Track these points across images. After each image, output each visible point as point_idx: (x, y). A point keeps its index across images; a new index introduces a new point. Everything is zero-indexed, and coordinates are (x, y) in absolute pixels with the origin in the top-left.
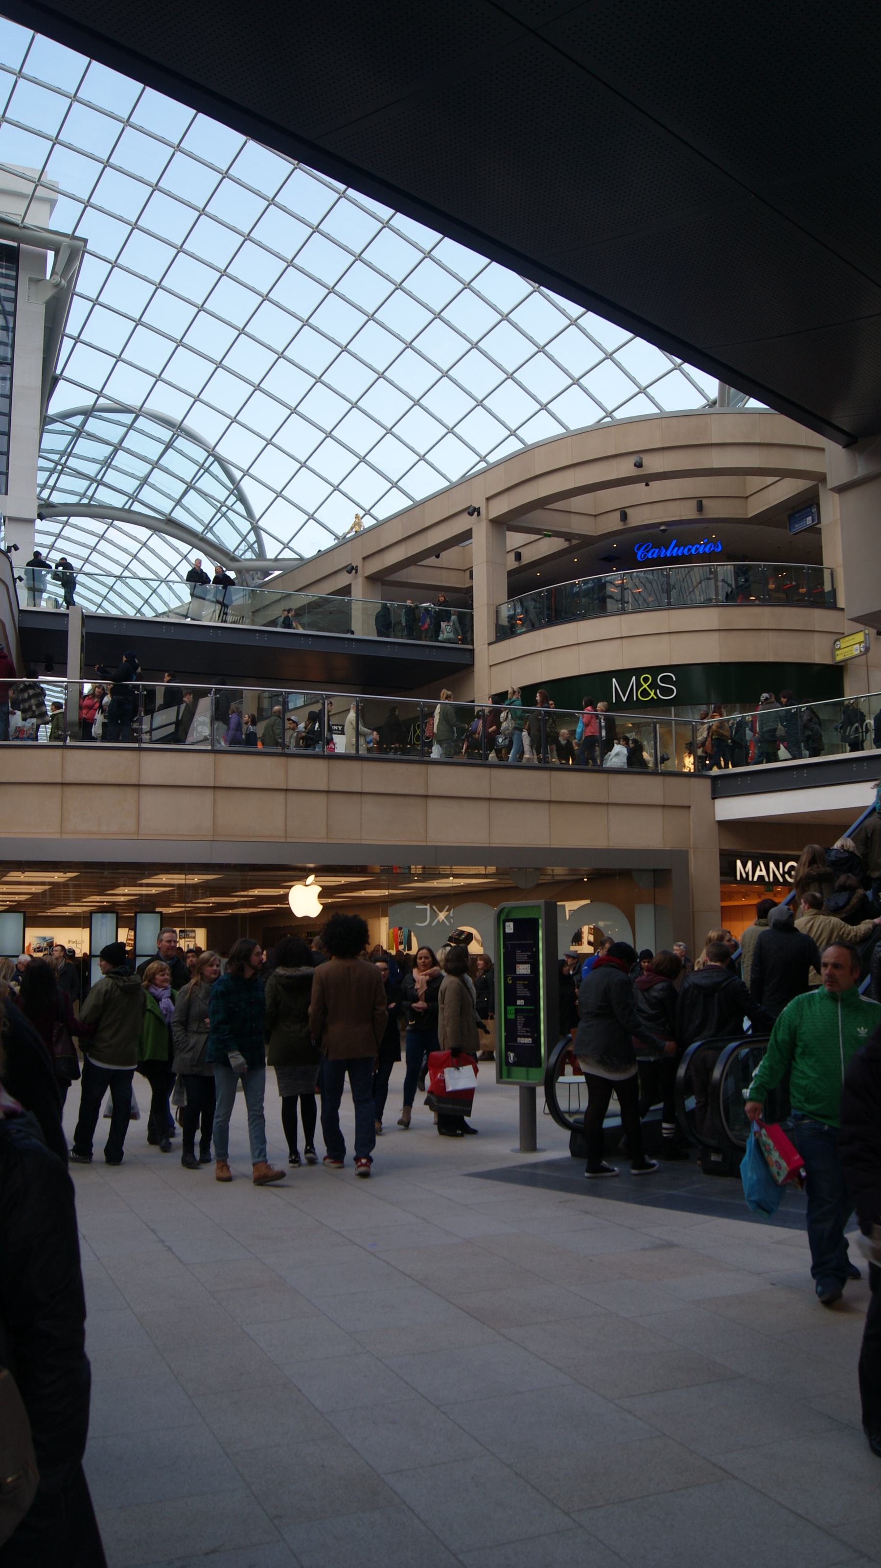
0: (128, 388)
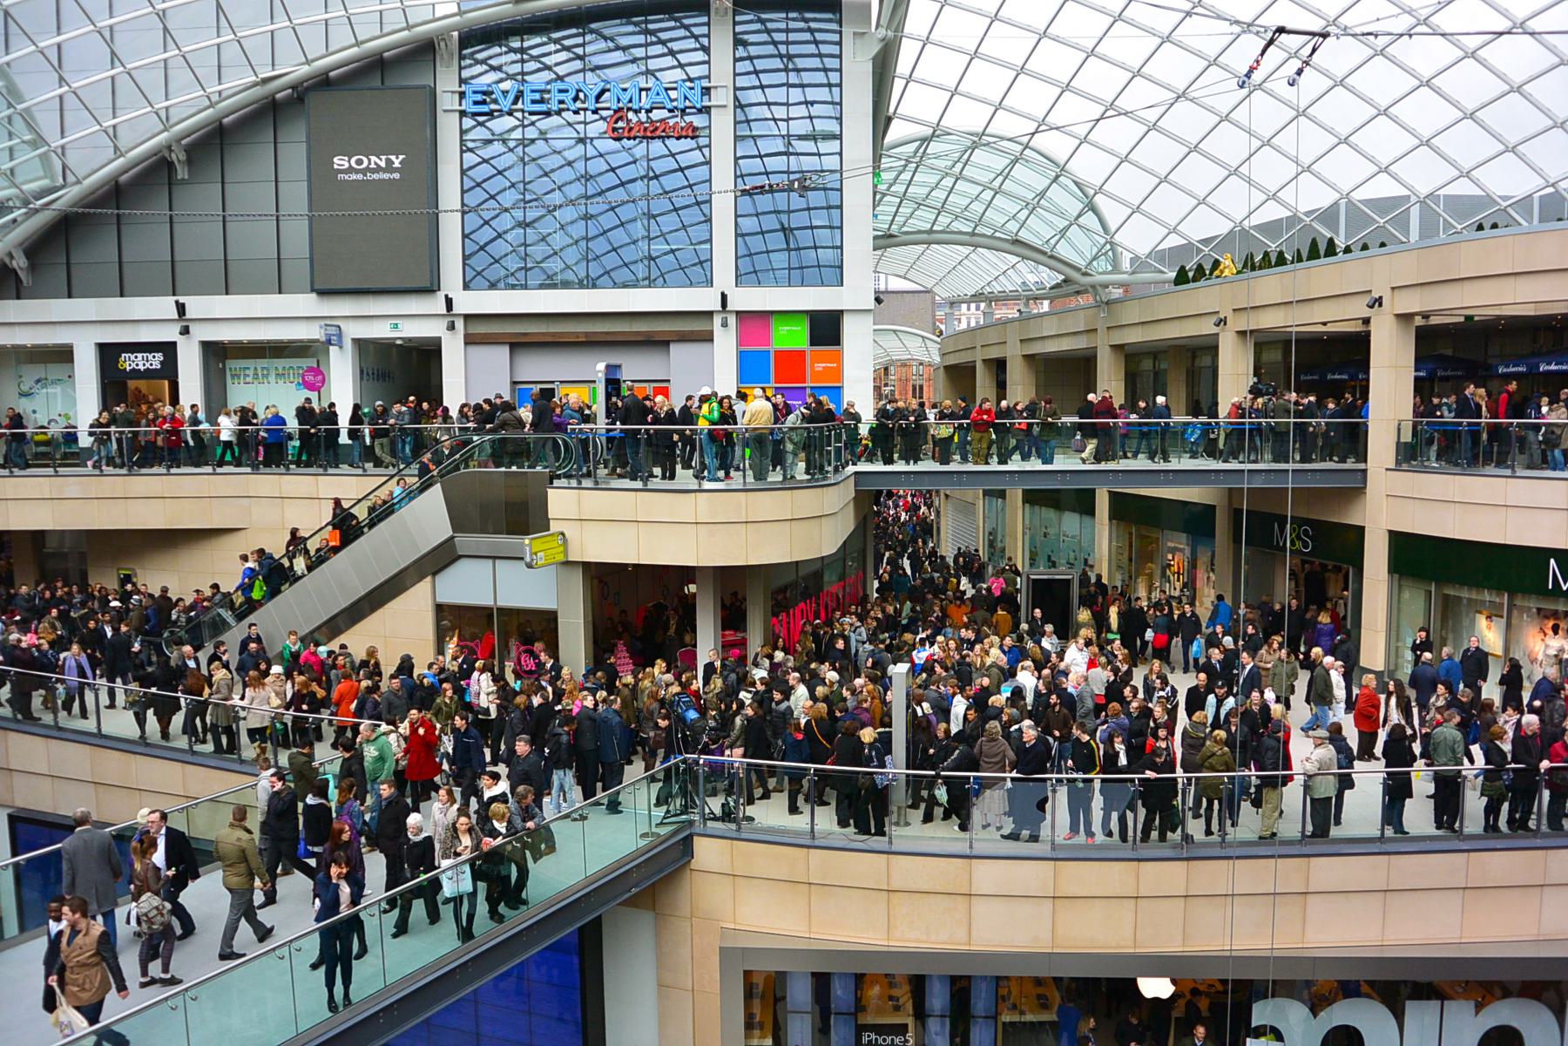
0: (966, 117)
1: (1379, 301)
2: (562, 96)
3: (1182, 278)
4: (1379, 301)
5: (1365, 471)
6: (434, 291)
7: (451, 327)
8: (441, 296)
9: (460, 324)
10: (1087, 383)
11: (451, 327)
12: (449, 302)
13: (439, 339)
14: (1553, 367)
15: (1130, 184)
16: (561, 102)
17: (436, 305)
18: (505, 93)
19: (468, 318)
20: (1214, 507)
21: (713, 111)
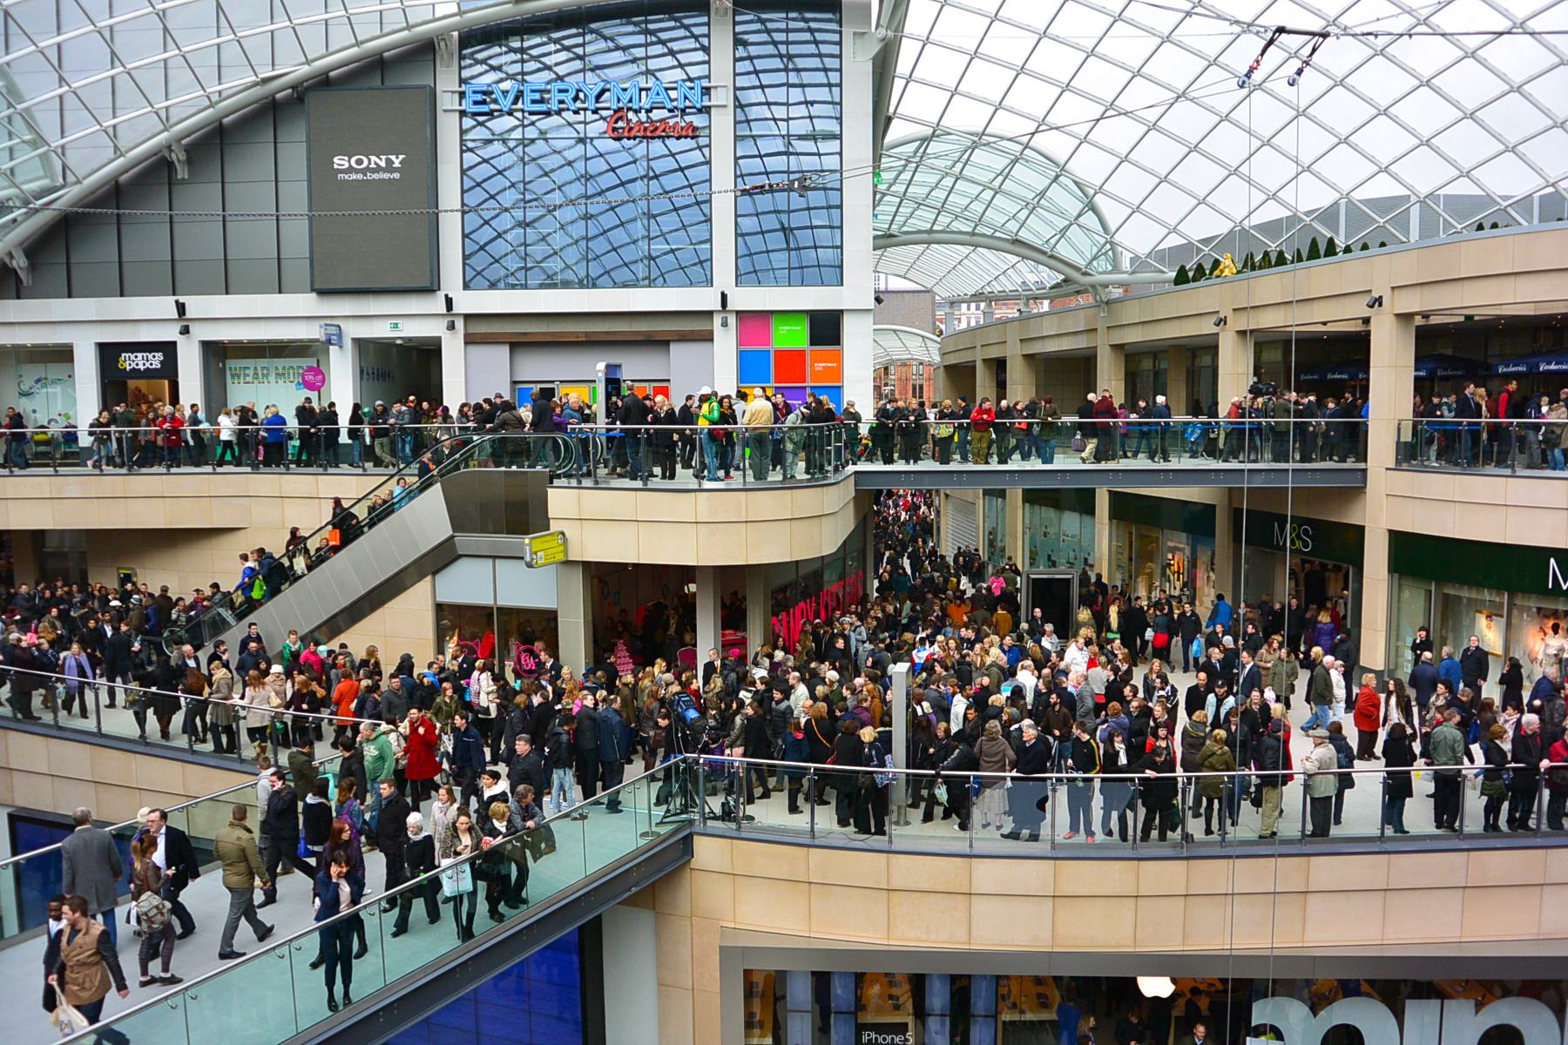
0: (966, 117)
1: (1379, 301)
2: (562, 96)
3: (1182, 278)
4: (1379, 301)
5: (1365, 471)
6: (434, 291)
7: (451, 327)
8: (441, 295)
9: (460, 324)
10: (1087, 383)
11: (451, 327)
12: (449, 302)
13: (439, 338)
14: (1553, 367)
15: (1130, 184)
16: (561, 102)
17: (436, 304)
18: (505, 93)
19: (468, 317)
20: (1214, 506)
21: (713, 111)
